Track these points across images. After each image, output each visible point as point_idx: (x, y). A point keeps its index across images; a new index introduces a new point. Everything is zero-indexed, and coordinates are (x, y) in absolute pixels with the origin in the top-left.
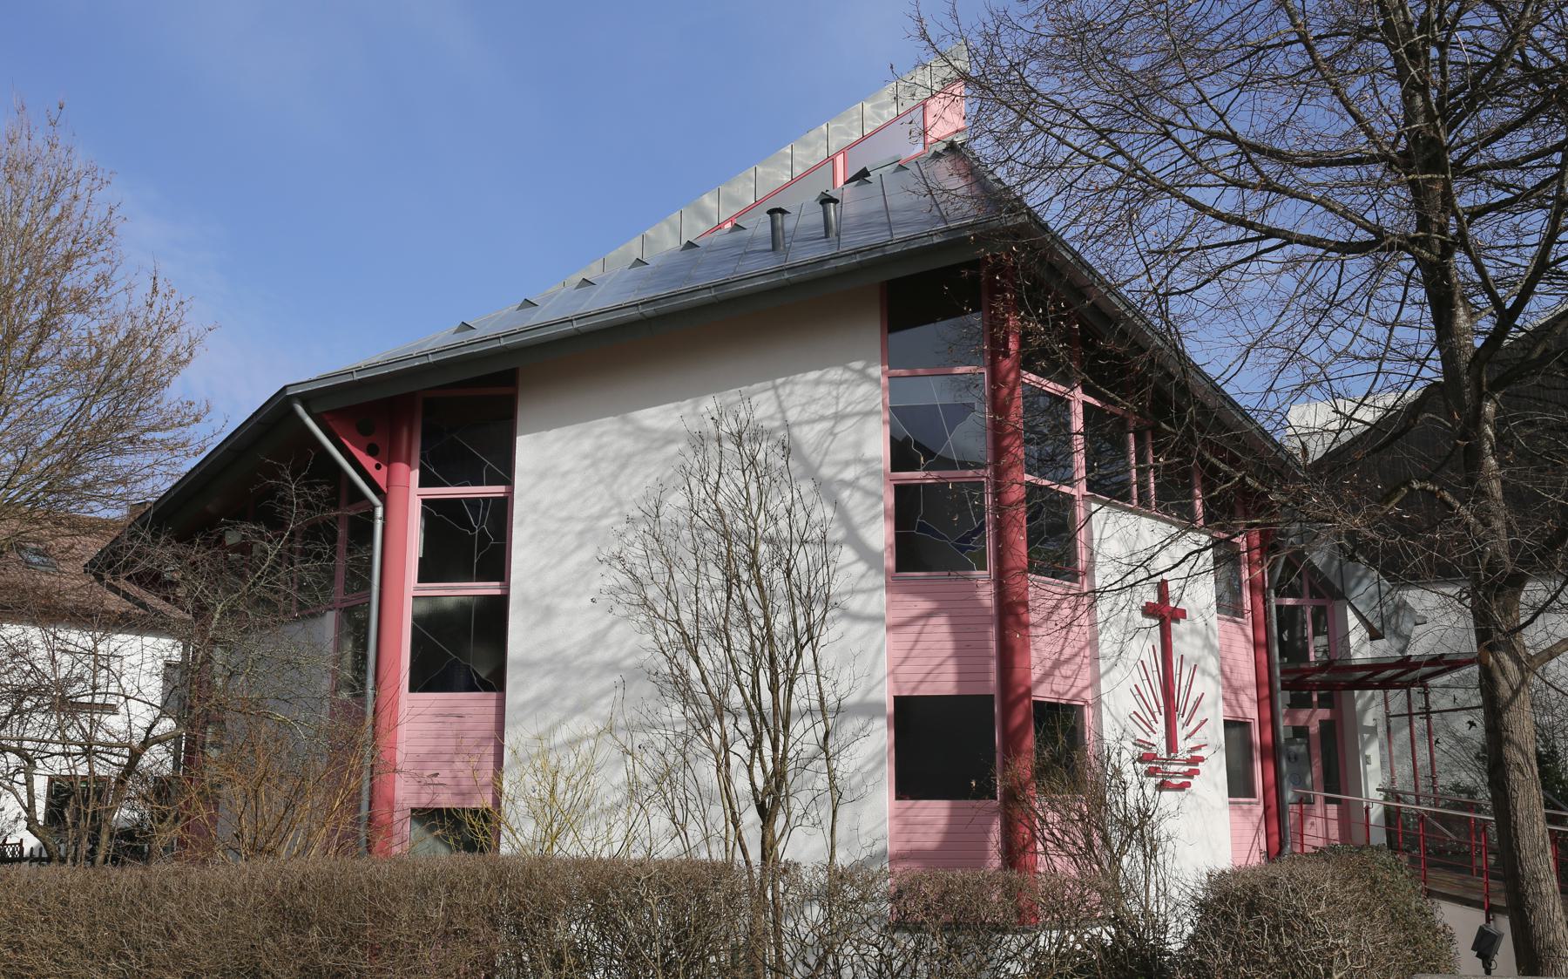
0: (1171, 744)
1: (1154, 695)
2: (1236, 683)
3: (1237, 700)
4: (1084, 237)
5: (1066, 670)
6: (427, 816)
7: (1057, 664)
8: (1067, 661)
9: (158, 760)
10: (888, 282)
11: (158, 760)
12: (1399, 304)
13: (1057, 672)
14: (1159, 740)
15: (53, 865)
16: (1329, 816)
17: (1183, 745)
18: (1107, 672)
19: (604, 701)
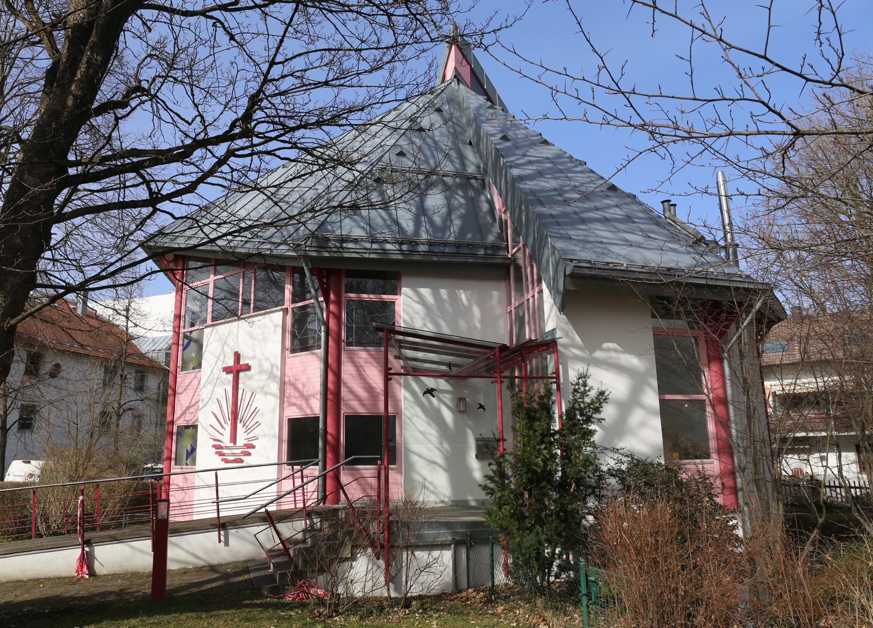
0: (234, 439)
1: (227, 410)
2: (305, 393)
3: (308, 404)
4: (362, 282)
5: (192, 410)
6: (57, 366)
7: (188, 408)
8: (193, 406)
9: (20, 134)
10: (396, 294)
11: (20, 134)
12: (799, 72)
13: (188, 412)
14: (226, 440)
15: (33, 539)
16: (291, 488)
17: (241, 440)
18: (203, 407)
19: (289, 599)
